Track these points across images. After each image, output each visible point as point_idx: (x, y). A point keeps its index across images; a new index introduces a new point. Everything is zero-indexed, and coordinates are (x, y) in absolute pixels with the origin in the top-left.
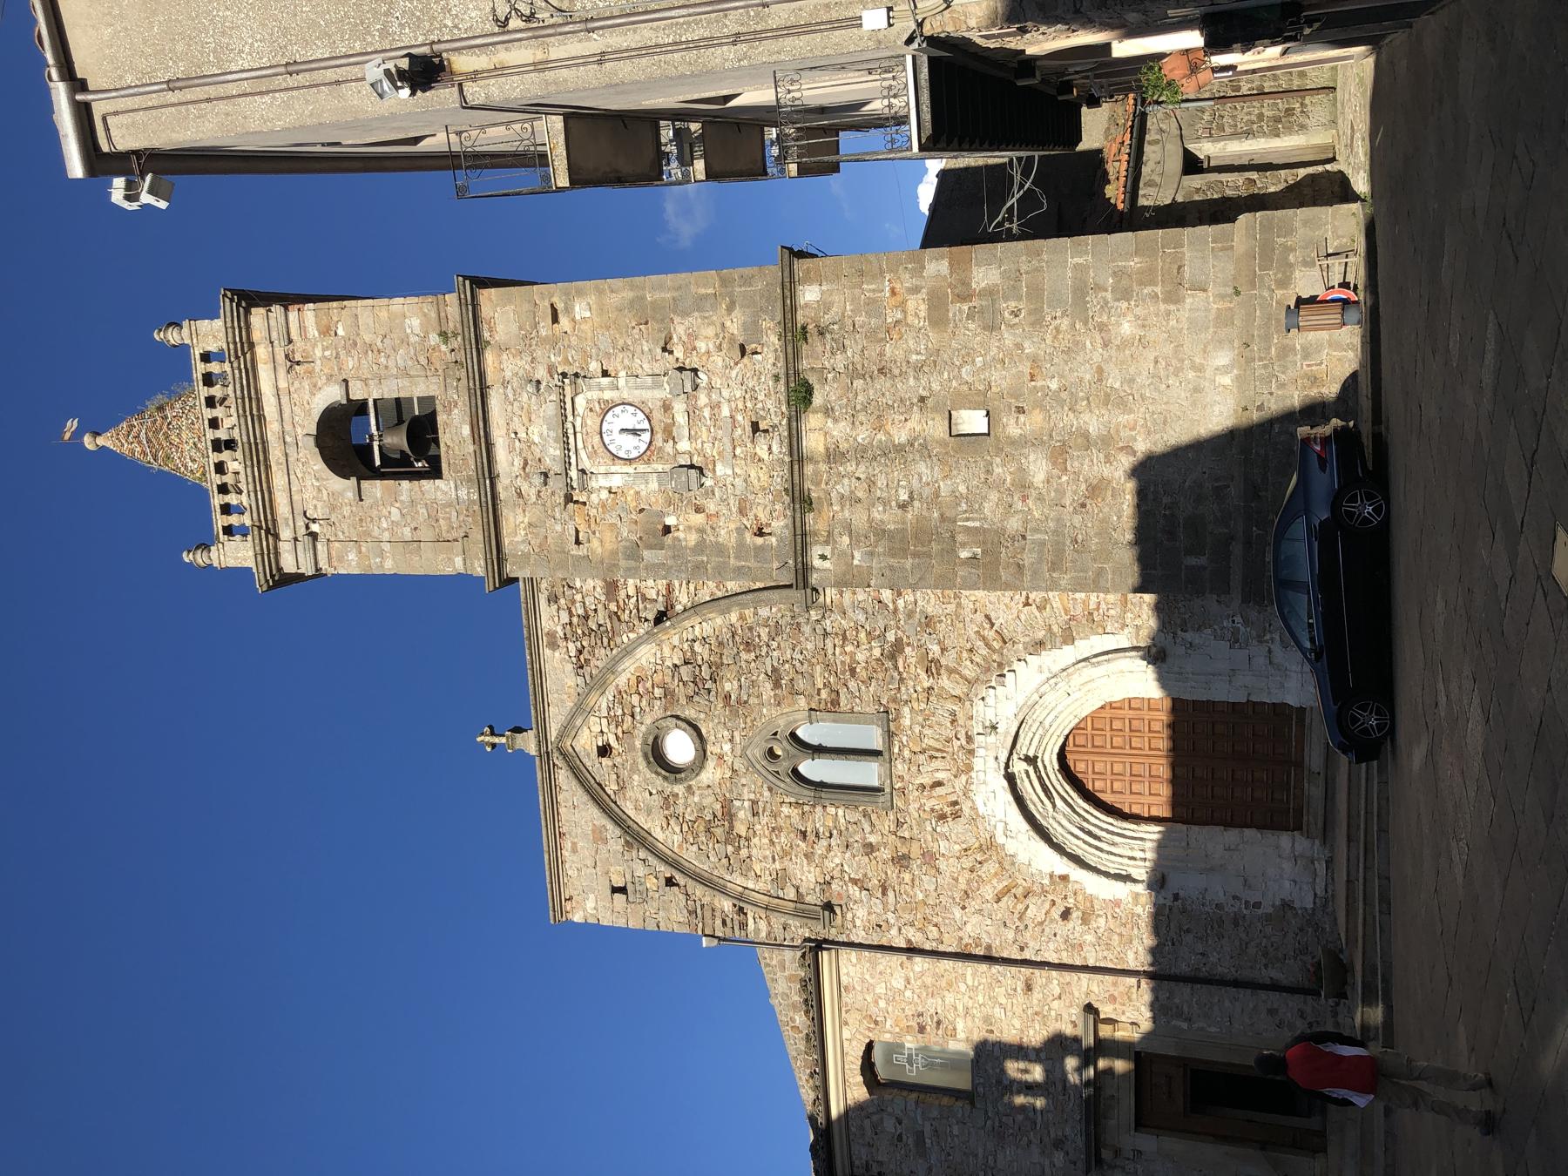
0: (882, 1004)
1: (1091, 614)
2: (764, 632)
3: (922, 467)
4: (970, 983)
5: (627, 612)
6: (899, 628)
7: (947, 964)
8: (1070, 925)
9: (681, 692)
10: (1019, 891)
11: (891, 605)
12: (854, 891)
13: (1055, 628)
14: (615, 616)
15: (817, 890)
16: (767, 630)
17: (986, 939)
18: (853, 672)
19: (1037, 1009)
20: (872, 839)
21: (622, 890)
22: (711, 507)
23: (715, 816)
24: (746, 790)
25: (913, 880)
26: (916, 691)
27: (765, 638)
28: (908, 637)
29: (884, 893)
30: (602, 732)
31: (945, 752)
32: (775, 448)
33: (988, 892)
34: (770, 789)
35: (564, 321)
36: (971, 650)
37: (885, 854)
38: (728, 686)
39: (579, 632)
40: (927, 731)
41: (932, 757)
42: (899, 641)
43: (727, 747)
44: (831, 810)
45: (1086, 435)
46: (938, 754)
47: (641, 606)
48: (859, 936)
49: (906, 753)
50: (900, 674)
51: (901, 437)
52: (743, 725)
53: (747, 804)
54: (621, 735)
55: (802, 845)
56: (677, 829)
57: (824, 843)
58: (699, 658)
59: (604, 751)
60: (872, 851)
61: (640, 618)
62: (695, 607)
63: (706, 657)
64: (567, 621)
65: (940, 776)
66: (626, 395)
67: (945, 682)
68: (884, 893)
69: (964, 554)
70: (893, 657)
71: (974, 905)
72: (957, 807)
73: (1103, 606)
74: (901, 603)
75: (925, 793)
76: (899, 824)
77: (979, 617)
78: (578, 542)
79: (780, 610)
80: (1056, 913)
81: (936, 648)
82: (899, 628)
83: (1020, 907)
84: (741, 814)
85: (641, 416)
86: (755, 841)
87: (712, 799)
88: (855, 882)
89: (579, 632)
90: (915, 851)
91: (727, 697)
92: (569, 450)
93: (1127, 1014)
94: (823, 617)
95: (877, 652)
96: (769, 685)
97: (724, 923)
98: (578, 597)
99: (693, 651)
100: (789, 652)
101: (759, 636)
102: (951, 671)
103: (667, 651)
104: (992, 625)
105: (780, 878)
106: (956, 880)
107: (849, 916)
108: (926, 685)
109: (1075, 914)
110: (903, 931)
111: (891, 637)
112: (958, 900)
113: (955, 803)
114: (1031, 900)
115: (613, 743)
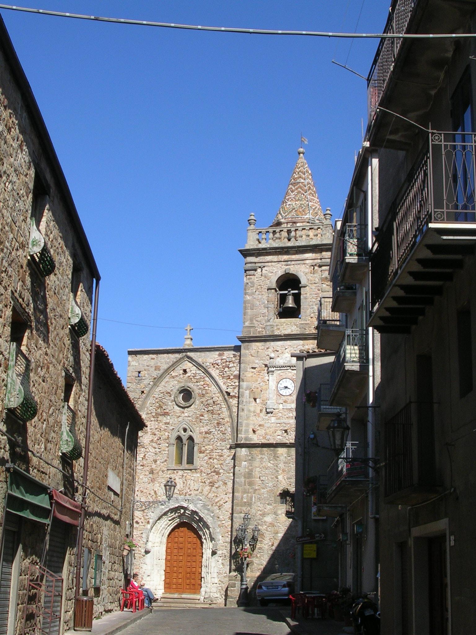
2: (223, 429)
3: (270, 484)
5: (230, 382)
9: (204, 399)
18: (210, 458)
20: (158, 462)
23: (164, 409)
27: (221, 429)
29: (141, 465)
32: (279, 437)
34: (173, 429)
36: (217, 496)
37: (154, 466)
38: (205, 416)
39: (224, 365)
42: (220, 474)
46: (185, 485)
49: (185, 475)
51: (280, 477)
55: (156, 439)
56: (160, 396)
57: (157, 446)
58: (215, 406)
61: (228, 386)
70: (215, 472)
76: (163, 471)
81: (217, 486)
84: (165, 419)
86: (157, 423)
88: (145, 456)
89: (224, 365)
90: (155, 476)
91: (202, 416)
95: (216, 466)
96: (206, 430)
111: (221, 471)
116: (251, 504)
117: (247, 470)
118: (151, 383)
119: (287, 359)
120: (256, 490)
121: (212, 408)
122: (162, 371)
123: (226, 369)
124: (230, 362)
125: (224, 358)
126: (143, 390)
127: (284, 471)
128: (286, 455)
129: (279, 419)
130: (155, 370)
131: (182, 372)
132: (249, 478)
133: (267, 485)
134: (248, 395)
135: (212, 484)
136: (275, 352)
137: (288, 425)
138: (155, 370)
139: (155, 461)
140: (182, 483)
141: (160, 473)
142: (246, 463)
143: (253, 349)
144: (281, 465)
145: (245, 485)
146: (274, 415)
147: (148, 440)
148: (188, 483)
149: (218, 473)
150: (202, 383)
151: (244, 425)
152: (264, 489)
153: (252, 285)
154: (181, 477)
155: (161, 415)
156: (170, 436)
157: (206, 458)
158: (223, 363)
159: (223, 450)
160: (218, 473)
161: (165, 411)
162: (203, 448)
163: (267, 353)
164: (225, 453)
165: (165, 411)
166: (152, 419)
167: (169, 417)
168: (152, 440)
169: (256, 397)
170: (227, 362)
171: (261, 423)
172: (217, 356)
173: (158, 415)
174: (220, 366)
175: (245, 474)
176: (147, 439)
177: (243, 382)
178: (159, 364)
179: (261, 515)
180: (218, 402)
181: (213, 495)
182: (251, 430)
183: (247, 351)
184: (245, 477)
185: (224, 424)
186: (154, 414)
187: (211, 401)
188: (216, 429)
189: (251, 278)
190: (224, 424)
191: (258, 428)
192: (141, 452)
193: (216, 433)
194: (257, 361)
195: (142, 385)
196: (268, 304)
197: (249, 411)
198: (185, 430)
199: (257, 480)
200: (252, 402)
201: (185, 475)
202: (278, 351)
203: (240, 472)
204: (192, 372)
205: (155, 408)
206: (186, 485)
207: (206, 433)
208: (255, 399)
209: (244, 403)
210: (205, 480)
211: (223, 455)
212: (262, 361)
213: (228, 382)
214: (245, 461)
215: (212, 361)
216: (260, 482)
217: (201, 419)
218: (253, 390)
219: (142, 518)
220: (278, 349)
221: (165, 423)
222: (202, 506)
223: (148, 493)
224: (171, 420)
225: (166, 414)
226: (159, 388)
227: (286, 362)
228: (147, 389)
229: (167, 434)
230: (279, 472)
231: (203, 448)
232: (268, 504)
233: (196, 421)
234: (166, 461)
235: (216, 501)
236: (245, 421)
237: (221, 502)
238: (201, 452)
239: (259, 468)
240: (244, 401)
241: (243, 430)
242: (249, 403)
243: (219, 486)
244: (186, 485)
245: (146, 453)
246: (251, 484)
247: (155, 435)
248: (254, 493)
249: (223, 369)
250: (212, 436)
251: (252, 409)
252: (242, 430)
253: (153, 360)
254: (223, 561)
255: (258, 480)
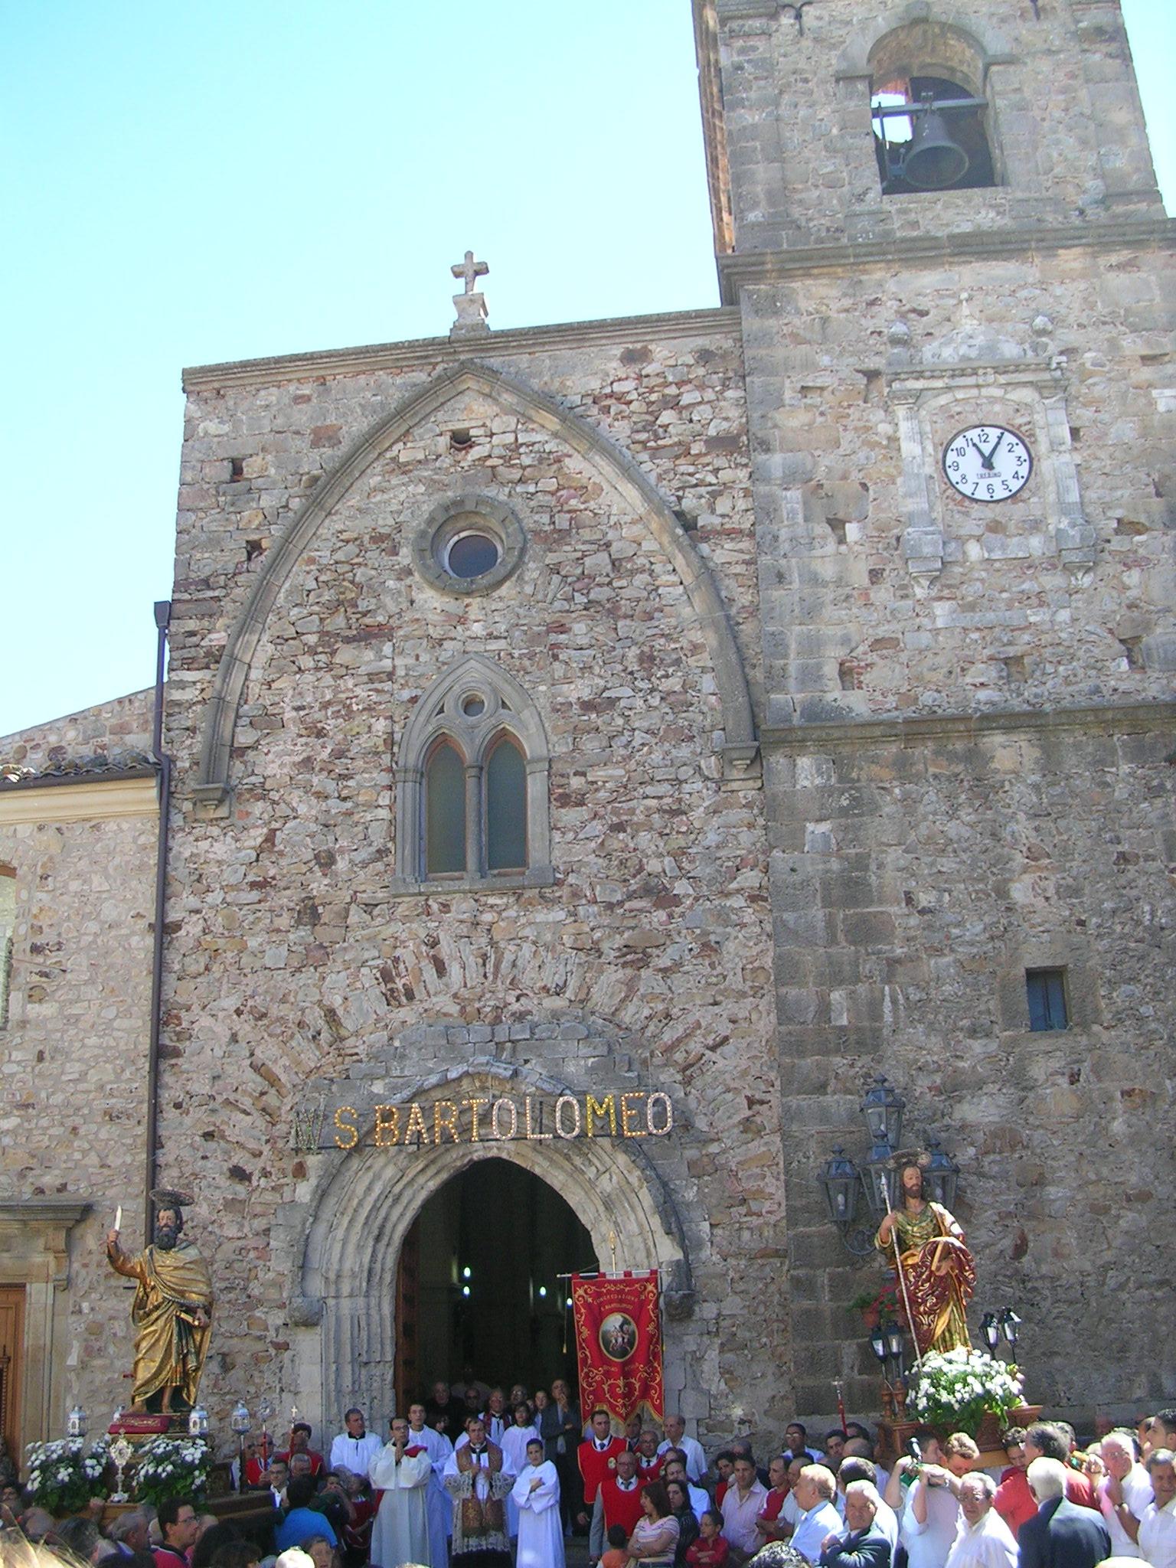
0: (75, 886)
1: (744, 1201)
2: (674, 684)
3: (975, 928)
4: (116, 1024)
5: (691, 469)
6: (697, 899)
7: (145, 987)
8: (223, 1181)
9: (565, 554)
10: (271, 1099)
11: (734, 886)
12: (257, 836)
13: (714, 1148)
14: (683, 450)
15: (253, 779)
16: (678, 688)
17: (186, 1046)
18: (619, 828)
19: (82, 1131)
20: (341, 865)
21: (237, 471)
22: (882, 594)
23: (364, 615)
24: (411, 661)
25: (278, 931)
26: (592, 930)
27: (665, 685)
28: (682, 916)
29: (253, 885)
30: (492, 435)
31: (496, 977)
32: (982, 695)
33: (267, 1051)
34: (414, 700)
35: (1146, 373)
36: (668, 1016)
37: (319, 885)
38: (579, 628)
39: (654, 397)
40: (527, 949)
41: (485, 957)
42: (676, 900)
43: (477, 629)
44: (385, 799)
45: (1040, 1182)
46: (490, 968)
47: (702, 490)
48: (183, 846)
49: (488, 917)
50: (621, 903)
51: (1020, 892)
52: (516, 653)
53: (387, 664)
54: (489, 463)
55: (325, 754)
56: (340, 556)
57: (331, 787)
58: (623, 583)
59: (462, 441)
60: (321, 865)
61: (682, 488)
62: (709, 576)
63: (626, 593)
64: (670, 379)
65: (454, 971)
66: (1045, 466)
67: (614, 975)
68: (253, 885)
69: (837, 996)
70: (647, 891)
71: (245, 1027)
72: (404, 1000)
73: (755, 1221)
74: (737, 902)
75: (424, 948)
76: (369, 907)
77: (725, 1028)
78: (805, 390)
79: (712, 709)
80: (239, 1159)
81: (665, 962)
82: (697, 899)
83: (246, 1103)
84: (369, 655)
85: (1015, 485)
86: (328, 679)
87: (392, 608)
88: (270, 838)
89: (654, 397)
90: (324, 934)
91: (562, 629)
92: (953, 376)
93: (83, 1272)
94: (707, 779)
95: (653, 865)
96: (586, 695)
97: (192, 634)
98: (709, 395)
99: (632, 573)
100: (645, 724)
101: (667, 676)
102: (631, 986)
103: (637, 530)
104: (713, 1048)
105: (269, 722)
106: (284, 1000)
107: (215, 831)
108: (605, 946)
109: (241, 1189)
110: (195, 917)
111: (681, 888)
112: (250, 1003)
113: (410, 995)
114: (261, 1122)
115: (476, 453)
116: (876, 1033)
117: (835, 865)
118: (295, 503)
119: (972, 342)
120: (898, 961)
121: (607, 592)
122: (344, 448)
123: (667, 417)
124: (679, 385)
125: (649, 369)
126: (254, 537)
127: (1032, 855)
128: (1035, 778)
129: (972, 607)
130: (315, 444)
131: (444, 441)
132: (852, 901)
133: (955, 931)
134: (799, 507)
135: (636, 956)
136: (912, 316)
137: (1026, 637)
138: (315, 444)
139: (326, 861)
140: (472, 961)
141: (355, 916)
142: (824, 827)
143: (798, 312)
144: (1022, 828)
145: (832, 941)
146: (946, 593)
147: (287, 759)
148: (508, 957)
149: (664, 898)
150: (552, 484)
151: (793, 646)
152: (939, 952)
153: (759, 73)
154: (464, 929)
155: (348, 640)
156: (397, 737)
157: (597, 827)
158: (651, 391)
159: (679, 782)
160: (664, 898)
161: (367, 620)
162: (576, 782)
163: (870, 324)
164: (694, 799)
165: (367, 620)
166: (307, 662)
167: (387, 649)
168: (308, 761)
169: (841, 515)
170: (666, 385)
171: (882, 631)
172: (615, 364)
173: (328, 640)
174: (634, 406)
175: (826, 885)
176: (279, 755)
177: (768, 450)
178: (331, 420)
179: (939, 1091)
180: (641, 561)
181: (646, 1012)
182: (831, 670)
183: (772, 322)
184: (827, 902)
185: (677, 662)
186: (312, 639)
187: (599, 561)
188: (639, 684)
189: (754, 49)
190: (677, 662)
191: (873, 657)
192: (251, 821)
193: (639, 703)
194: (825, 360)
195: (250, 516)
196: (842, 137)
197: (815, 580)
198: (471, 705)
199: (893, 909)
200: (824, 538)
201: (488, 917)
202: (923, 314)
203: (795, 878)
204: (495, 440)
205: (316, 608)
206: (497, 967)
207: (587, 706)
208: (837, 524)
209: (785, 547)
210: (597, 935)
211: (684, 807)
212: (851, 360)
213: (682, 469)
214: (820, 820)
215: (595, 384)
216: (914, 921)
217: (554, 646)
218: (820, 486)
219: (266, 1149)
220: (923, 303)
221: (372, 677)
222: (591, 1070)
223: (293, 1016)
224: (399, 662)
225: (369, 635)
226: (335, 524)
227: (973, 354)
228: (276, 531)
229: (381, 725)
230: (1014, 865)
231: (576, 782)
232: (973, 1032)
233: (531, 657)
234: (382, 853)
235: (668, 1037)
236: (797, 628)
237: (695, 1046)
238: (565, 800)
239: (900, 850)
240: (784, 534)
241: (792, 670)
242: (811, 546)
243: (678, 965)
244: (497, 967)
245: (275, 825)
246: (865, 932)
247: (320, 734)
248: (889, 979)
249: (651, 418)
250: (620, 721)
251: (827, 570)
252: (784, 669)
253: (304, 406)
254: (730, 1356)
255: (896, 910)
